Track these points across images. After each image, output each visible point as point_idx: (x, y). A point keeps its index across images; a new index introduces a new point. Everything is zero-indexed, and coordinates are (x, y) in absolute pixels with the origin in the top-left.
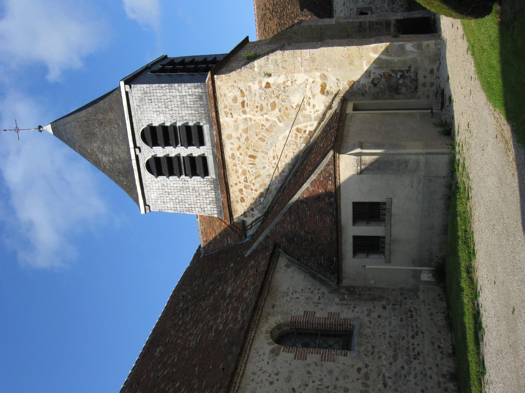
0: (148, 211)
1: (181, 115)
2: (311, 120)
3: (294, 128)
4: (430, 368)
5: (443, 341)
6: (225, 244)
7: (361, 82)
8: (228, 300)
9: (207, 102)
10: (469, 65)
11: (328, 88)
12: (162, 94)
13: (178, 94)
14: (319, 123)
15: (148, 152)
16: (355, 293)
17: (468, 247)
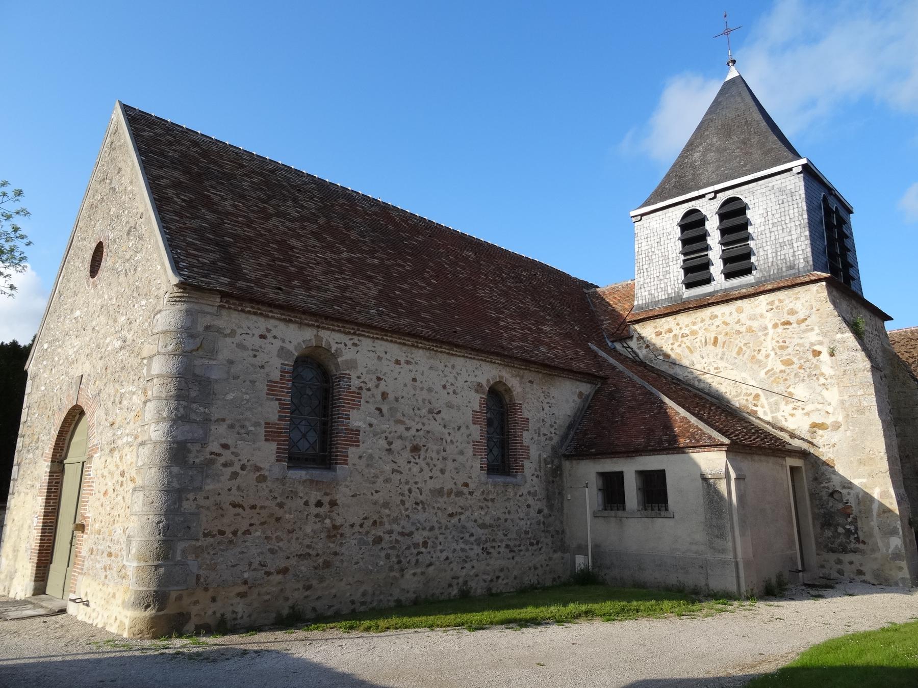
0: (634, 219)
1: (764, 245)
2: (772, 412)
3: (759, 392)
4: (473, 567)
5: (505, 582)
6: (602, 318)
7: (833, 476)
8: (534, 328)
9: (786, 276)
10: (868, 624)
11: (820, 432)
12: (792, 216)
13: (794, 237)
14: (768, 423)
15: (710, 209)
16: (554, 478)
17: (618, 613)
